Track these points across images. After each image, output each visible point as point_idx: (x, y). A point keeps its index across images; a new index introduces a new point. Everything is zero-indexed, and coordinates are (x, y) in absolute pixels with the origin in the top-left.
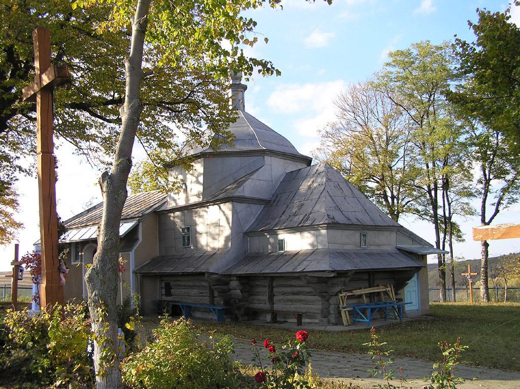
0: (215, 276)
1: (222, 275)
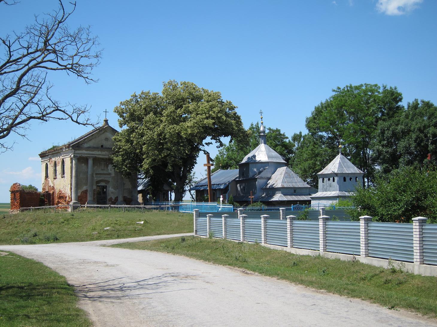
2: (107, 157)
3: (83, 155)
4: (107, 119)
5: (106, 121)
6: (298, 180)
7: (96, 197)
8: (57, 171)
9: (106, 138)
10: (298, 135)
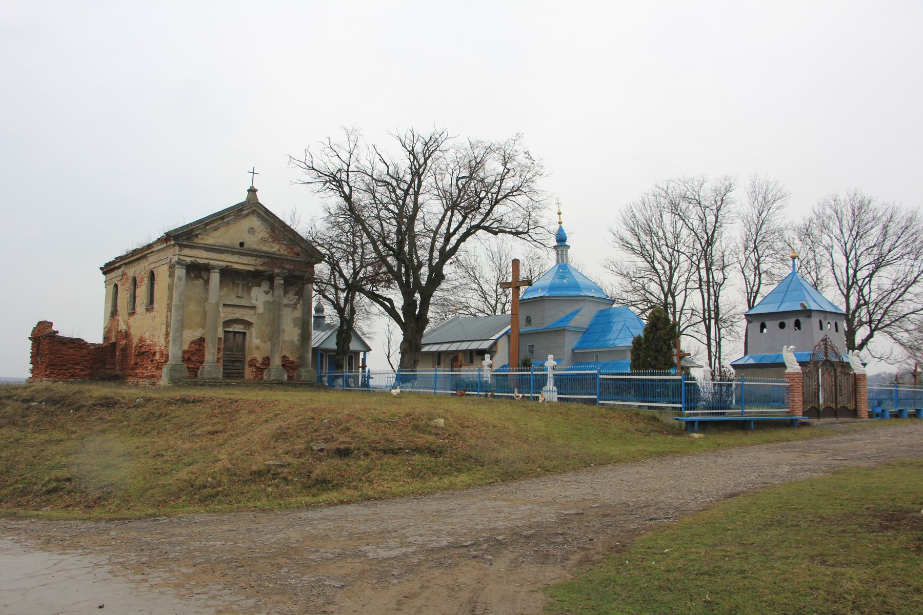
2: (252, 268)
3: (198, 259)
4: (256, 187)
5: (252, 191)
7: (222, 355)
8: (137, 299)
9: (251, 228)
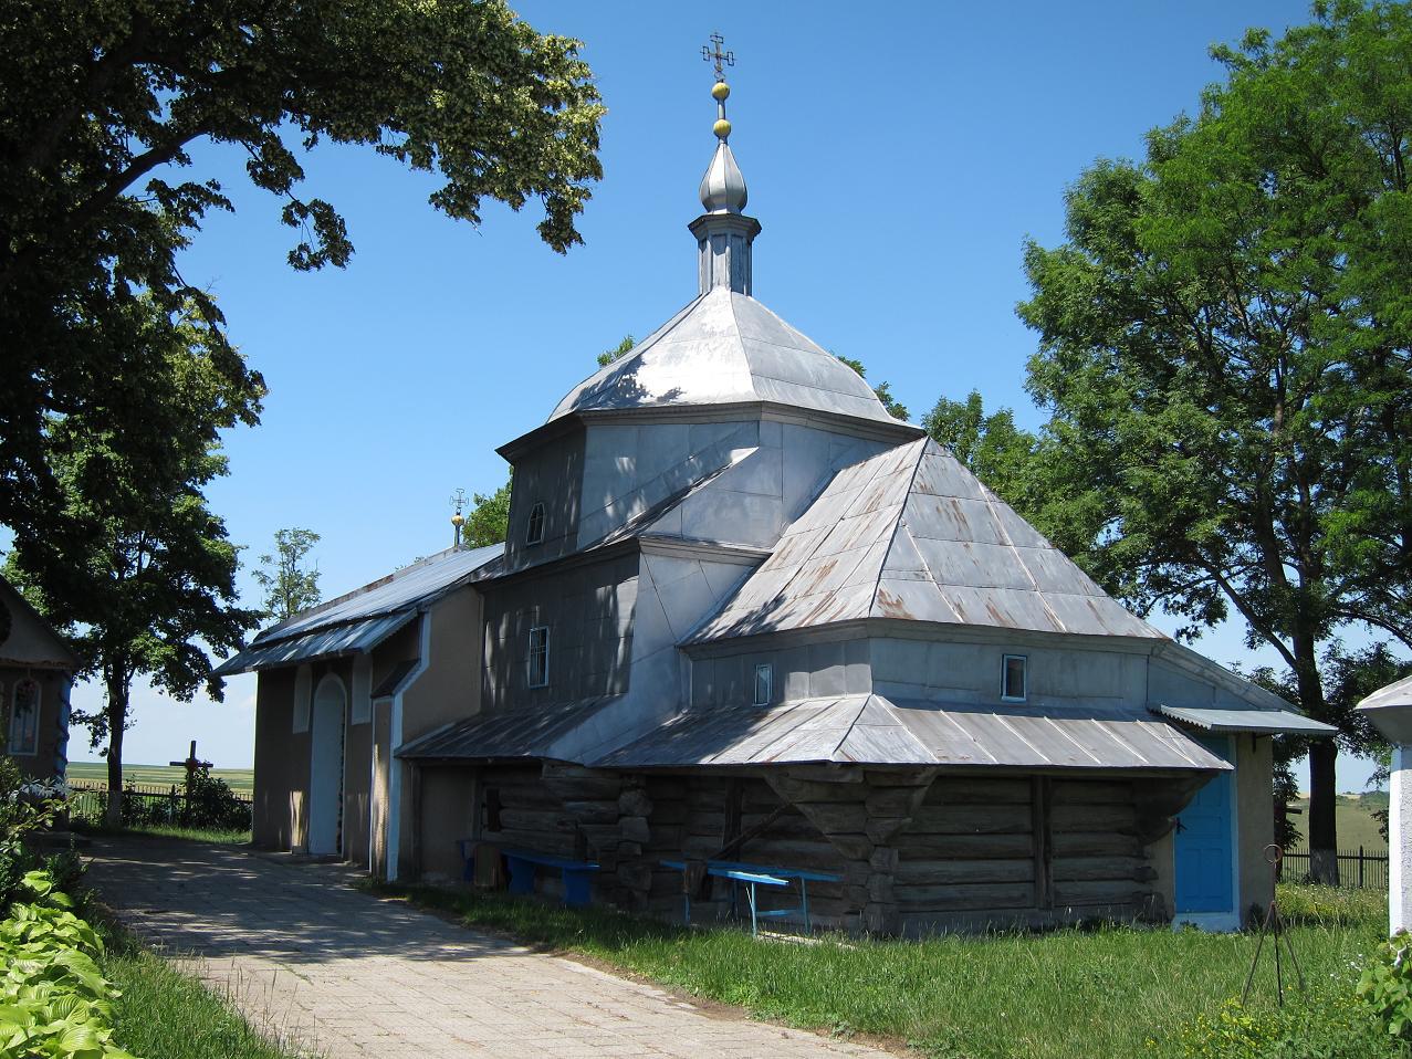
0: (574, 772)
1: (593, 768)
6: (1037, 570)
10: (957, 411)
